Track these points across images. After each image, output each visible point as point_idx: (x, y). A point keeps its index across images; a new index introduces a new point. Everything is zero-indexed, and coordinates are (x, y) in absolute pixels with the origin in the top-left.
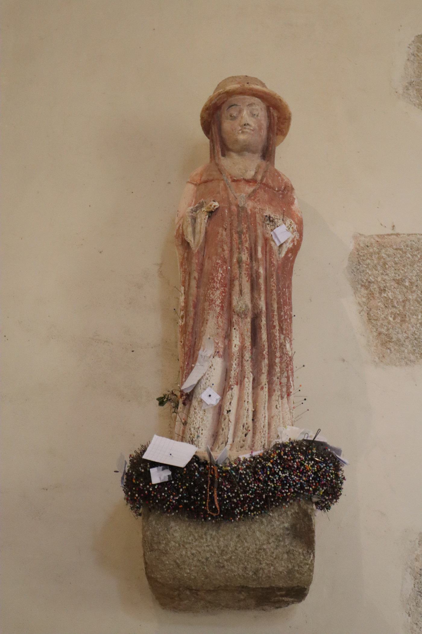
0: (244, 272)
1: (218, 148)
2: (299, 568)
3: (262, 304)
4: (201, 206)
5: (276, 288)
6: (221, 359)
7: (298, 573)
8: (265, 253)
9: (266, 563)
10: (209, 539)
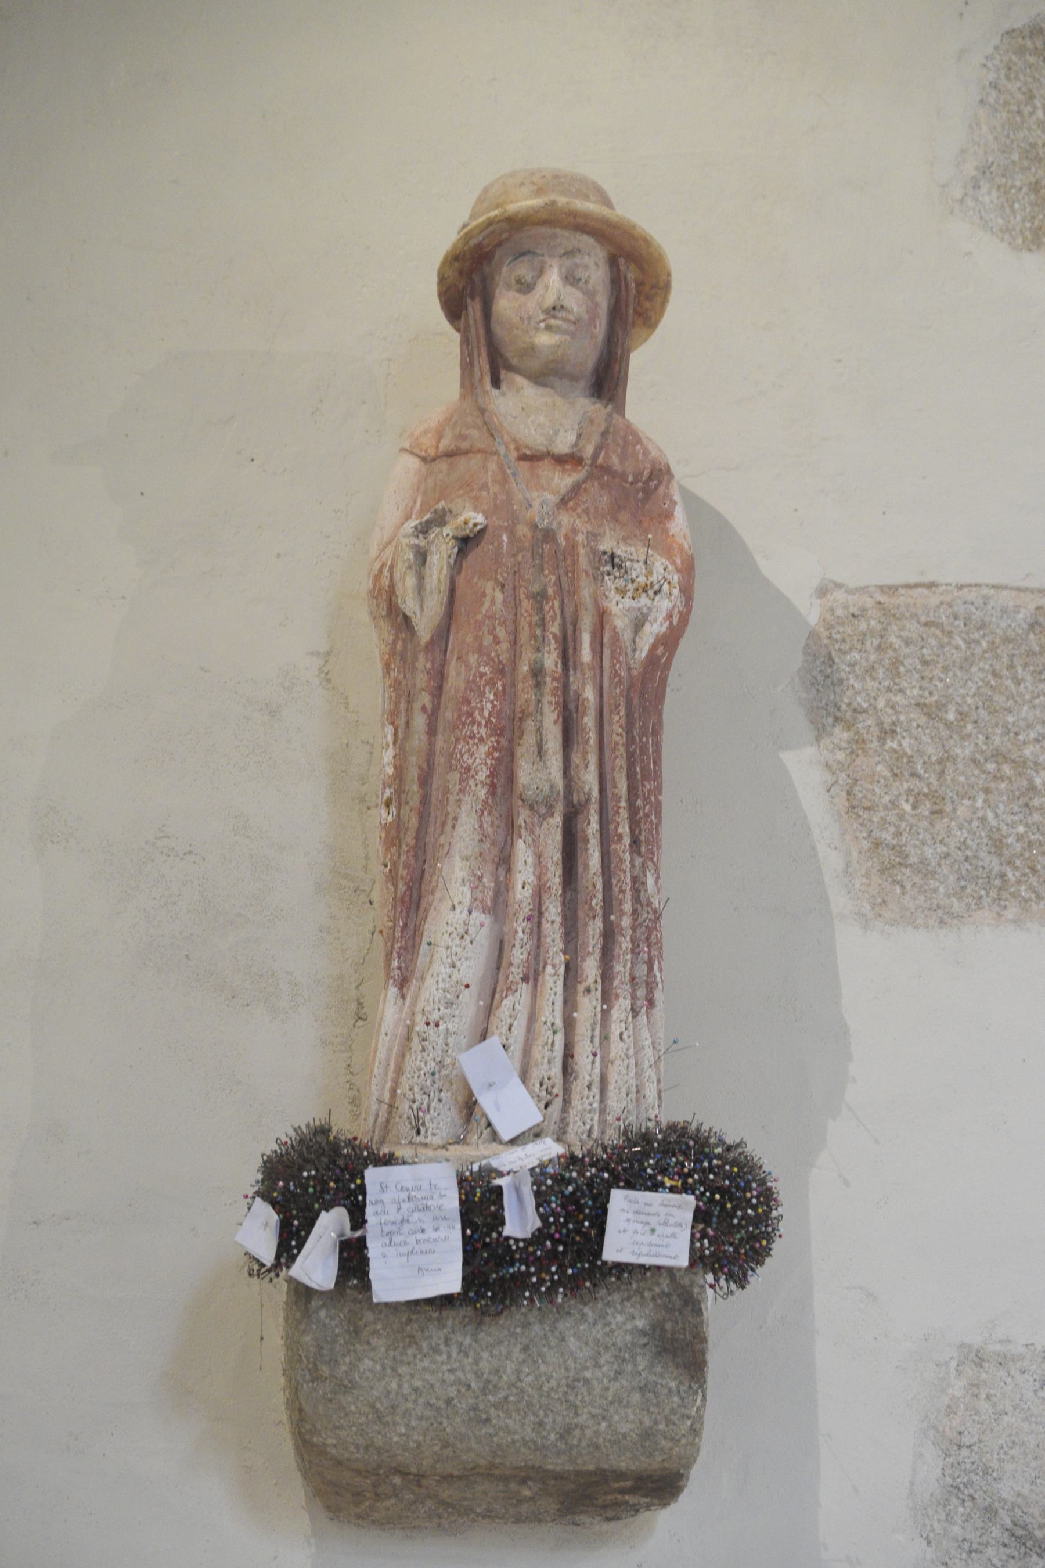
0: (548, 698)
1: (483, 363)
2: (667, 1426)
3: (589, 779)
4: (440, 519)
5: (625, 739)
6: (488, 916)
7: (665, 1438)
8: (598, 648)
9: (590, 1413)
10: (454, 1354)
